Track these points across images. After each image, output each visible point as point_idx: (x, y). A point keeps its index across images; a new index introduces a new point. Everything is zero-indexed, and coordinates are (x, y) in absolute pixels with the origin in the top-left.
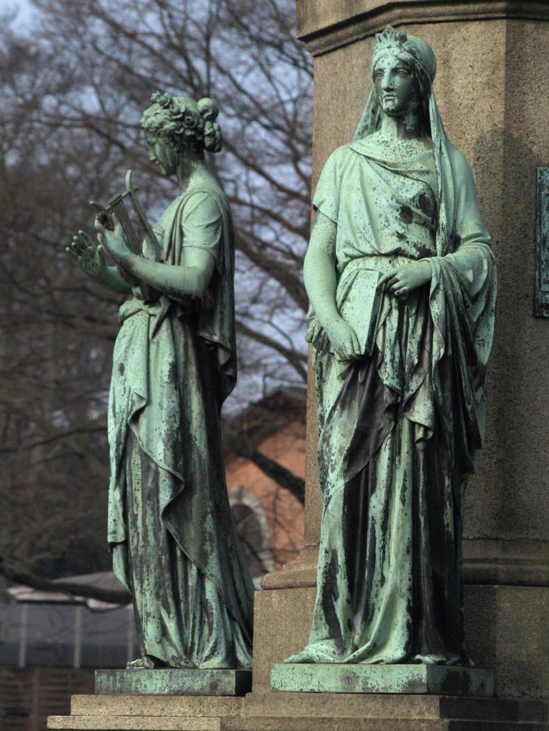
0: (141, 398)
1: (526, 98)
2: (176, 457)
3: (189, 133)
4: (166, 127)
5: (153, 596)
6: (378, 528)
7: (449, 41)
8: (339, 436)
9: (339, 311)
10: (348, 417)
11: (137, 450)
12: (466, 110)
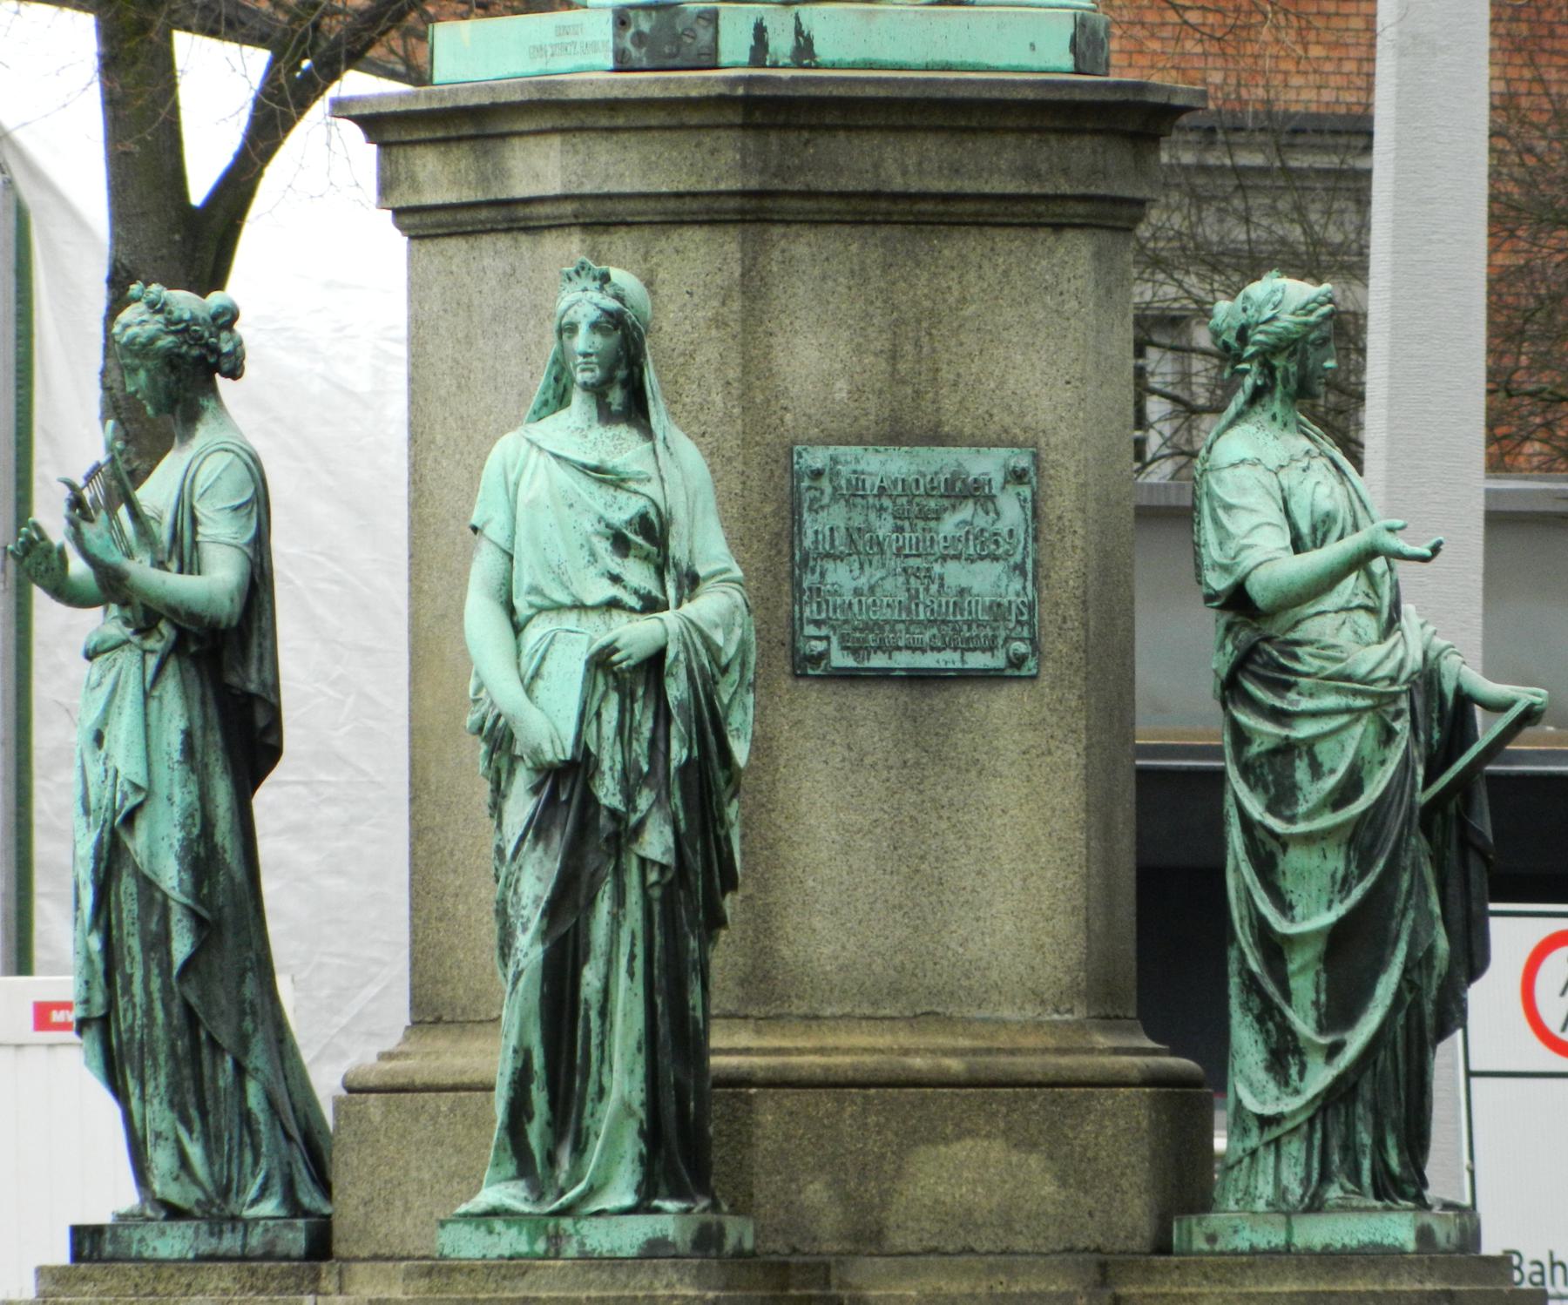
0: (137, 788)
1: (773, 340)
2: (198, 883)
3: (195, 352)
4: (160, 343)
5: (165, 1105)
6: (593, 1015)
7: (653, 253)
8: (533, 880)
9: (529, 690)
10: (546, 851)
11: (130, 870)
12: (681, 360)
